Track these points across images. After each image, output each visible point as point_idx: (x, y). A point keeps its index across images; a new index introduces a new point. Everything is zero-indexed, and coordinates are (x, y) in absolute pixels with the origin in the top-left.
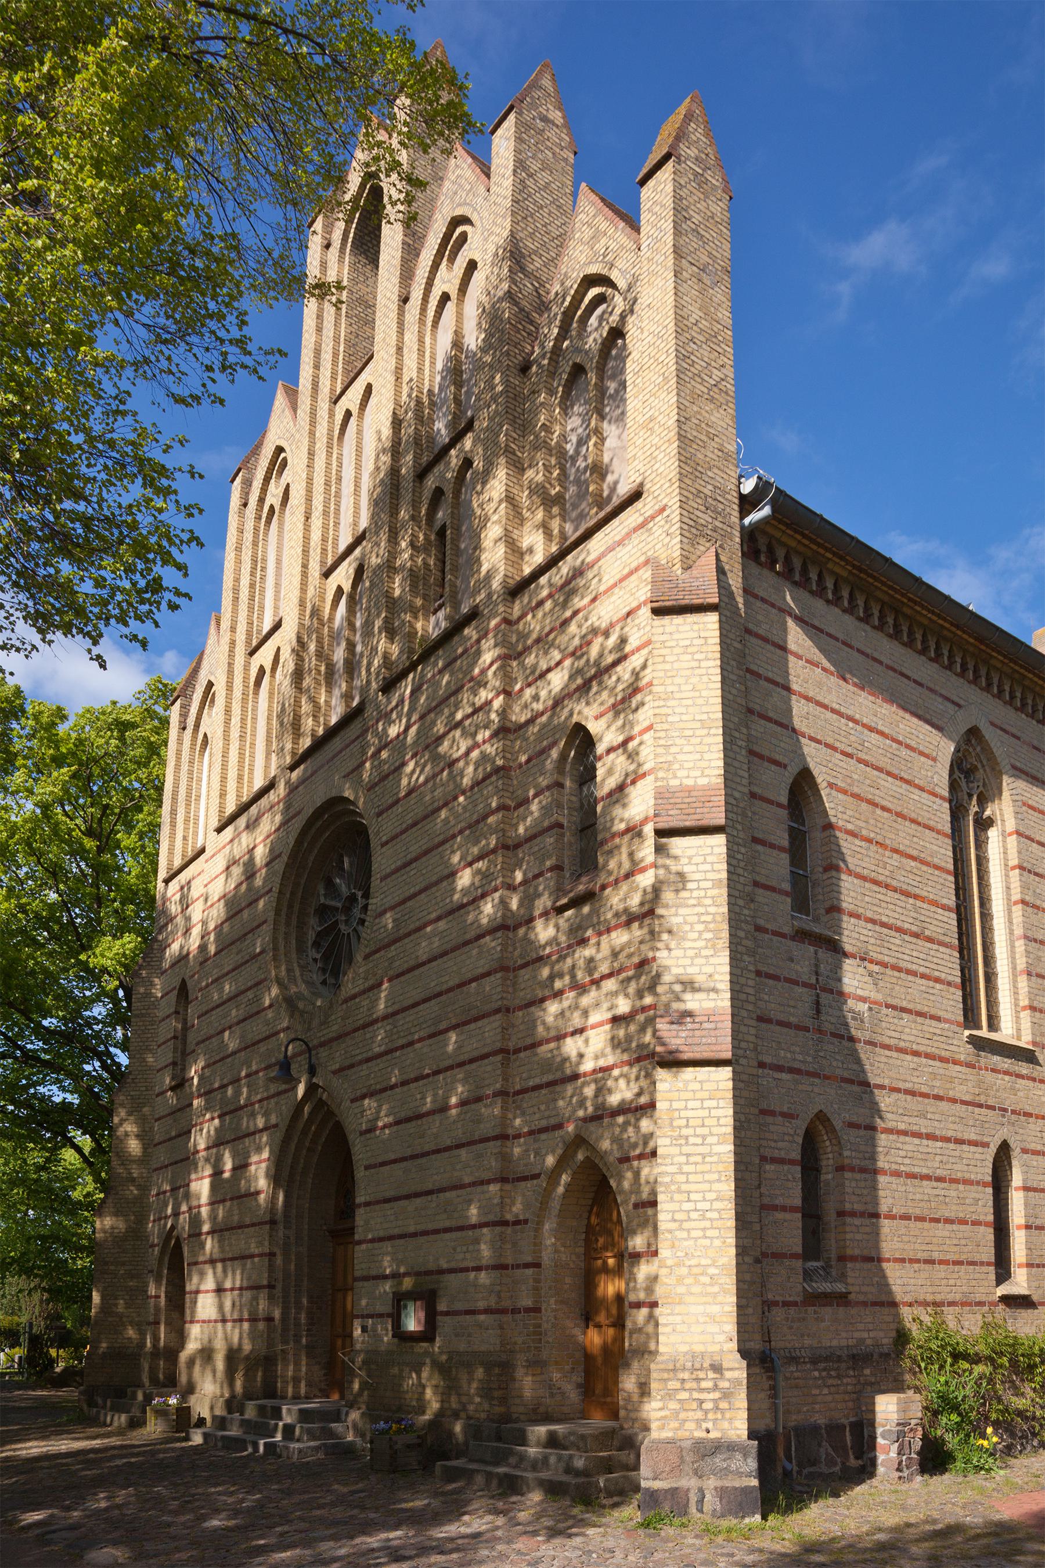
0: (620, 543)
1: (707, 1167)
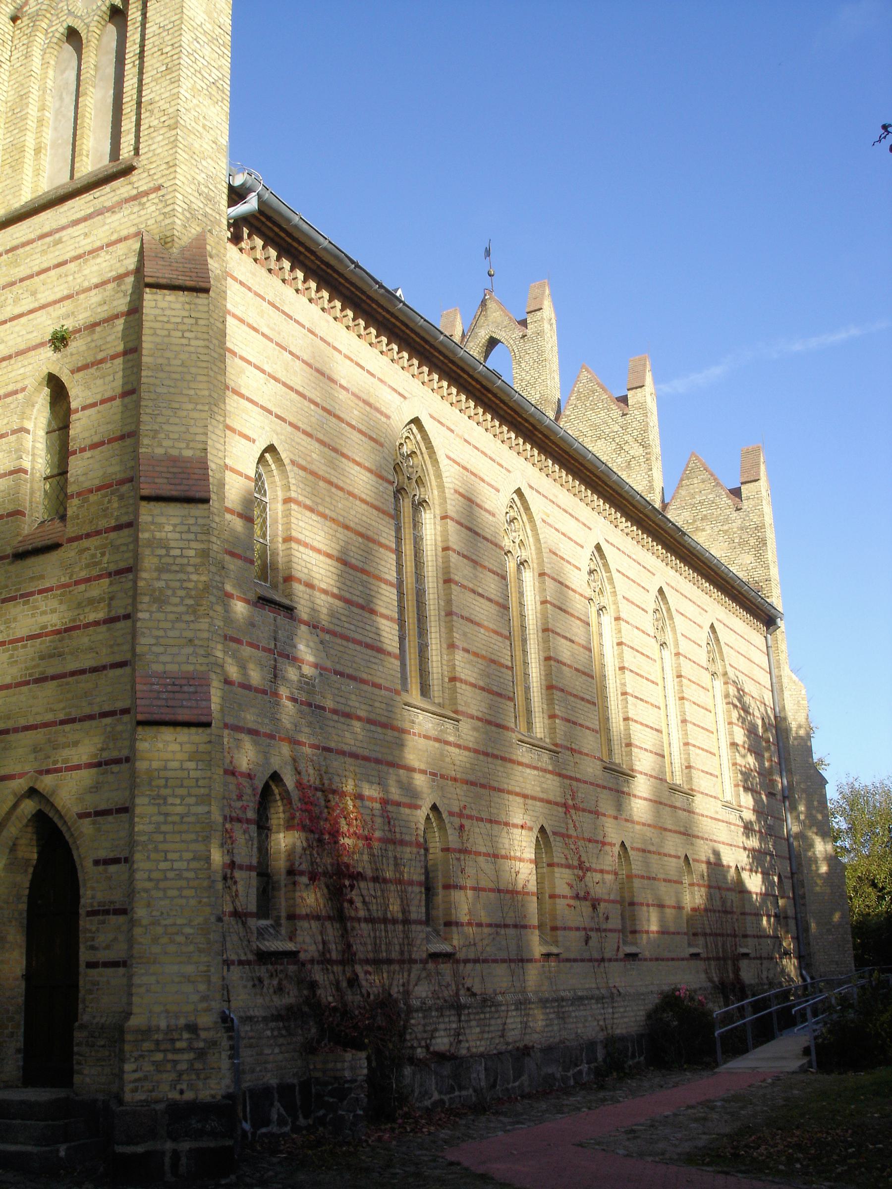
0: (111, 209)
1: (185, 827)
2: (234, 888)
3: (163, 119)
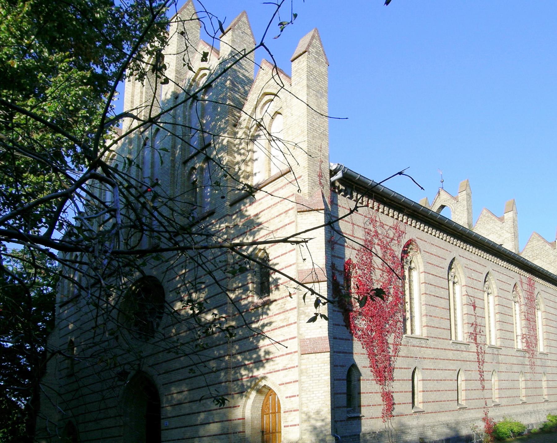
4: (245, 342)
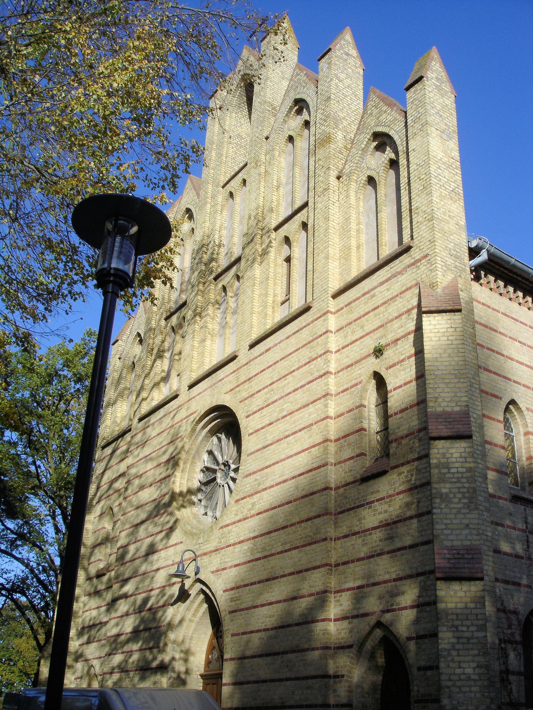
0: (400, 273)
2: (509, 687)
3: (424, 216)
4: (353, 542)
